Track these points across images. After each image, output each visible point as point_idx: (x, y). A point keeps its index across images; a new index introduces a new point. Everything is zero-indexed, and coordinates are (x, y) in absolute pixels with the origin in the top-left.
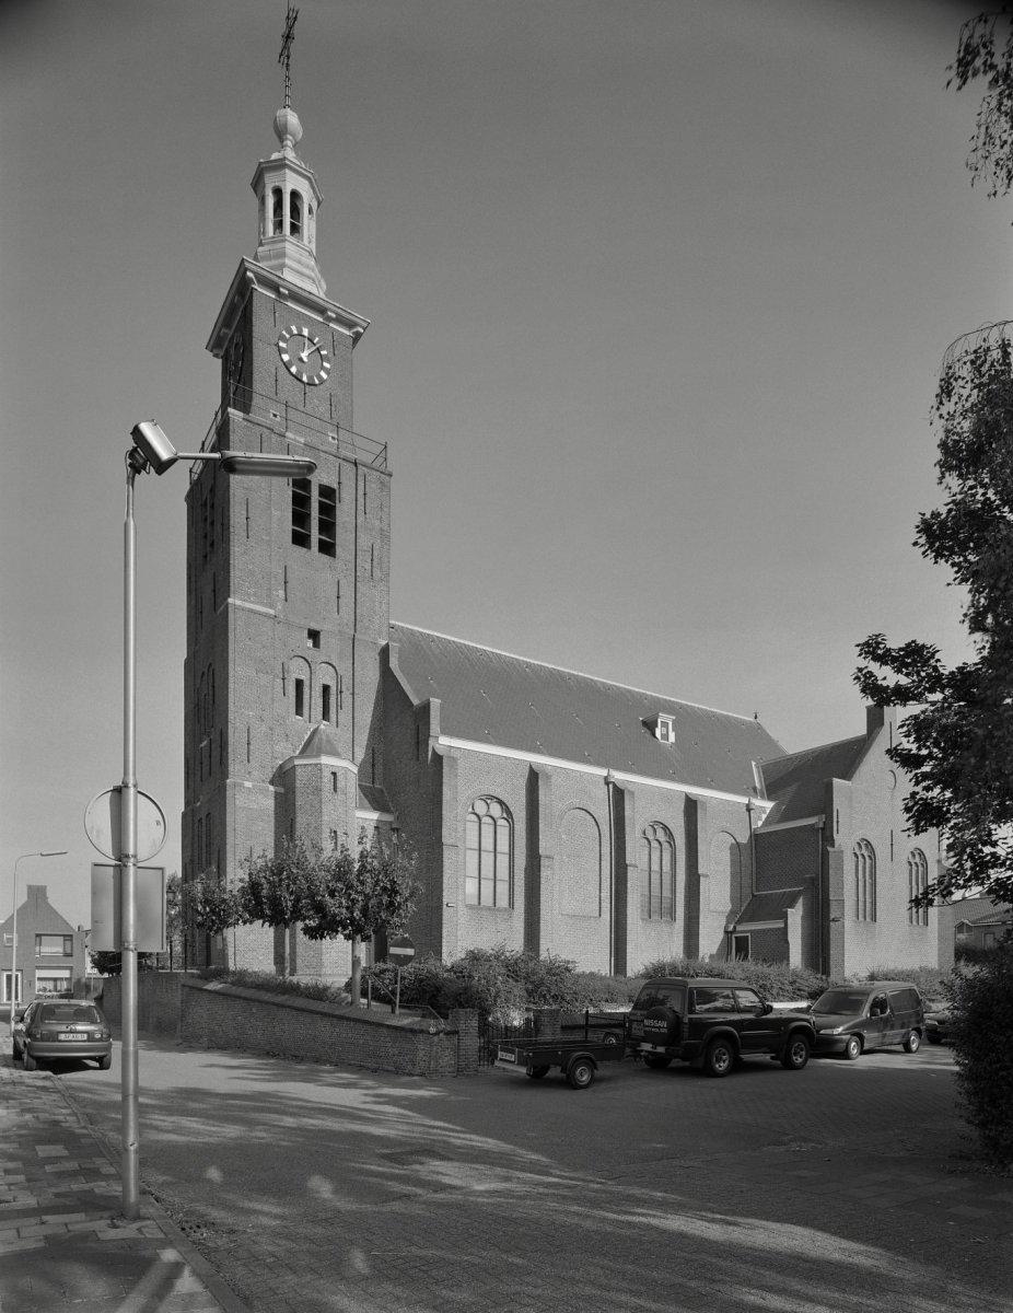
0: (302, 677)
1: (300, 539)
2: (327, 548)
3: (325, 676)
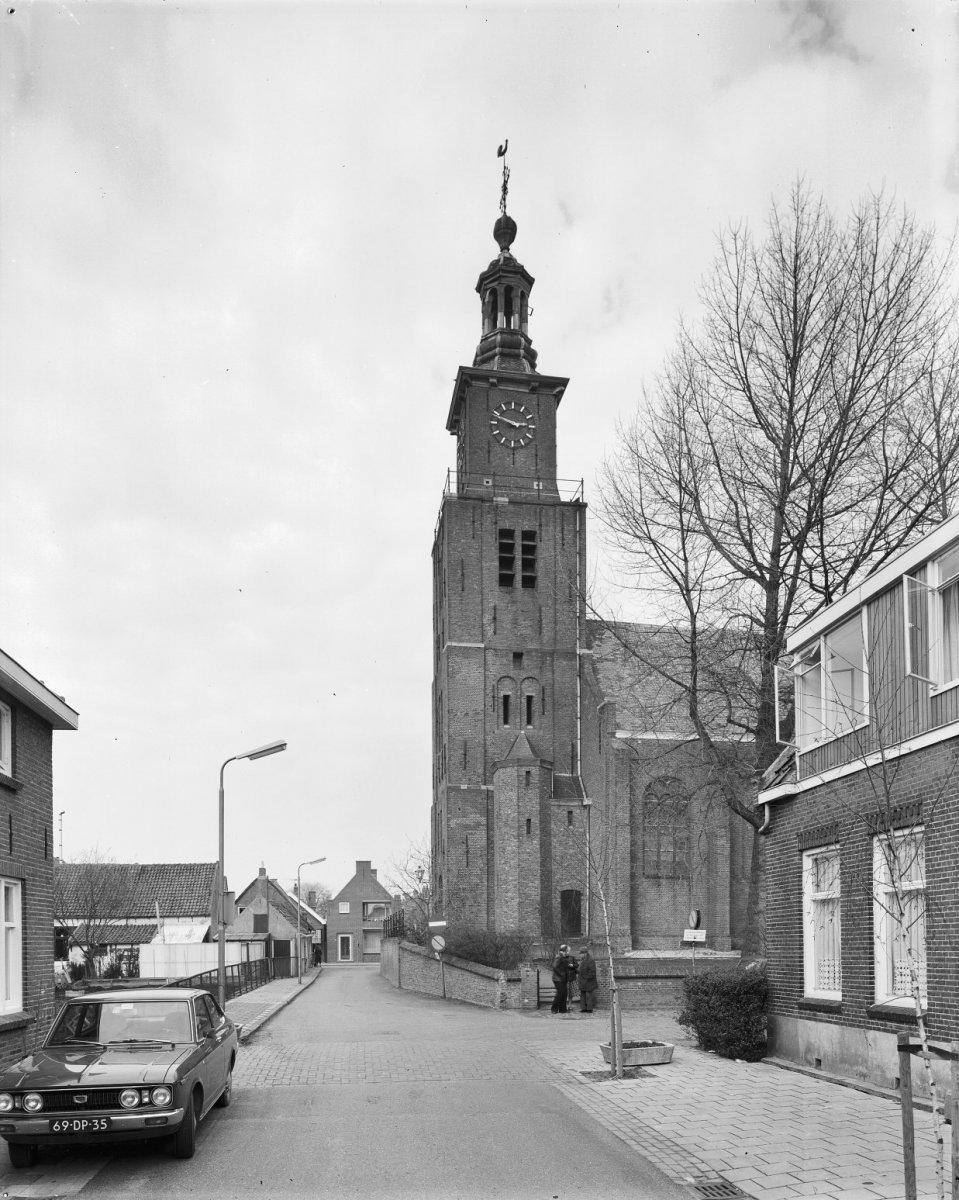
0: (533, 694)
1: (506, 581)
2: (529, 582)
3: (530, 689)
